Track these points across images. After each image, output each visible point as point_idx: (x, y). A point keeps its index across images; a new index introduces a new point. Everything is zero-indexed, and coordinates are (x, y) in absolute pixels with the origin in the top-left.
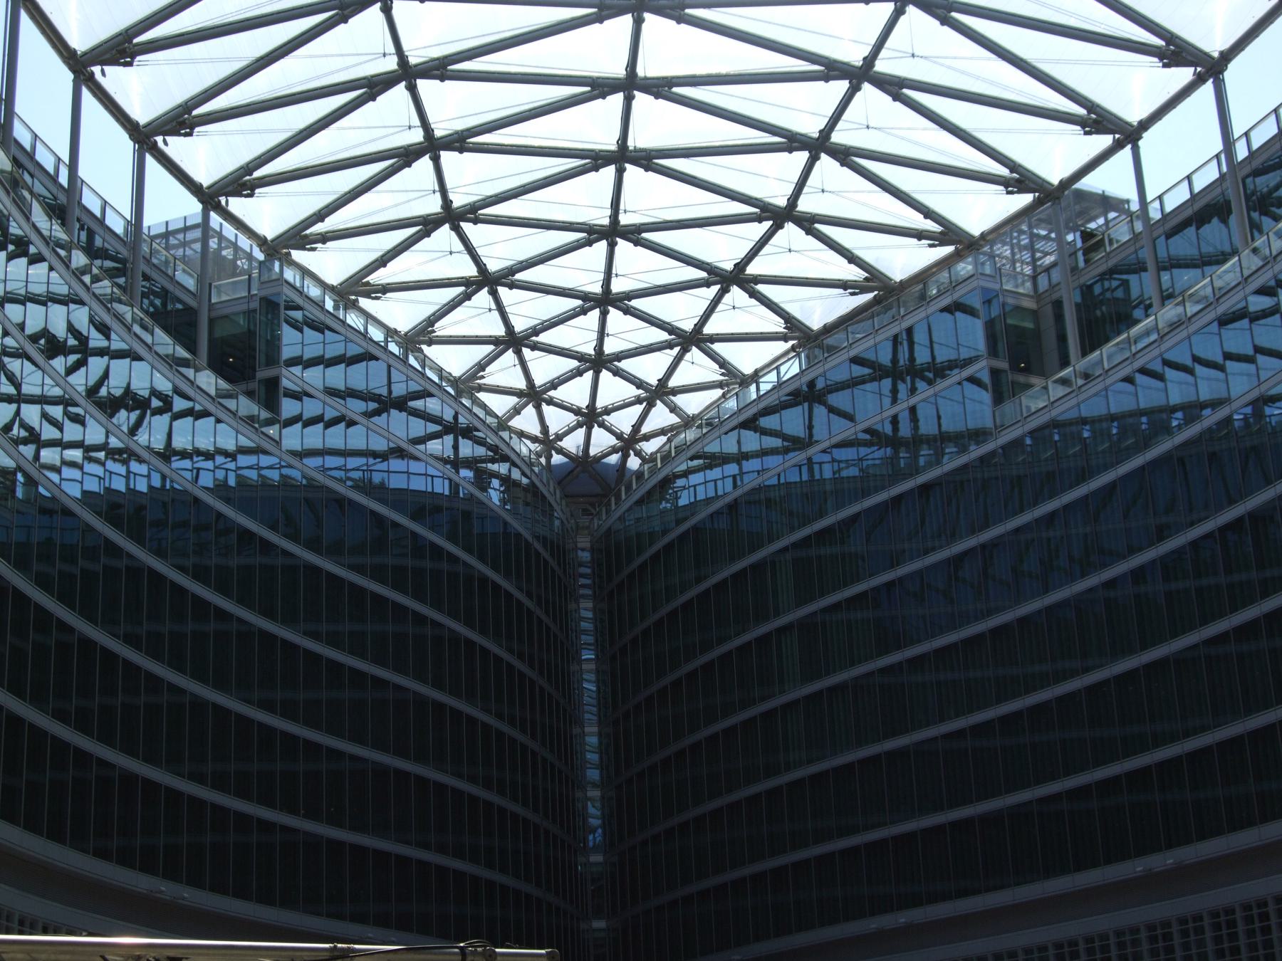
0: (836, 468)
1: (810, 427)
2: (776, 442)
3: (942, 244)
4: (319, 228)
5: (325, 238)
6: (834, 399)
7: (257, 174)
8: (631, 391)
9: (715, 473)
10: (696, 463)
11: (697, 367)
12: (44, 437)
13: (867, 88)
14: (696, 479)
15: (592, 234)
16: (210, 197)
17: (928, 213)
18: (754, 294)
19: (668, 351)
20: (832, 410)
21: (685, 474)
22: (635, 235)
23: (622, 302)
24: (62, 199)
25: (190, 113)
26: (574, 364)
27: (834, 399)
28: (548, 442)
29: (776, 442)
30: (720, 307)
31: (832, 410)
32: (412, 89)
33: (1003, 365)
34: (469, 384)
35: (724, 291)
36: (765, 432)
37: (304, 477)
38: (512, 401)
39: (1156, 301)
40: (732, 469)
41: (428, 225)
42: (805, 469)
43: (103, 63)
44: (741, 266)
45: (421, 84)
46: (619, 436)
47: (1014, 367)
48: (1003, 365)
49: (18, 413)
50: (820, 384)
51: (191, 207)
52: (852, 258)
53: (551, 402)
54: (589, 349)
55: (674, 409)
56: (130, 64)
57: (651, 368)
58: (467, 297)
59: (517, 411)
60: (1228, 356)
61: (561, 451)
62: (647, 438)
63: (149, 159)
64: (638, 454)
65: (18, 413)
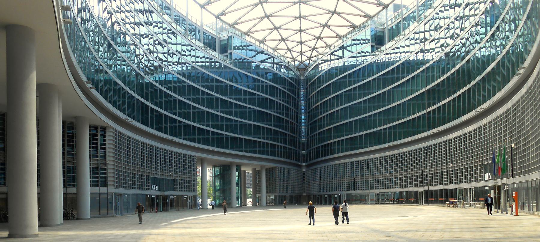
0: (348, 63)
1: (343, 54)
2: (337, 57)
6: (348, 48)
8: (309, 49)
9: (326, 64)
10: (322, 62)
11: (320, 43)
13: (335, 14)
14: (322, 65)
15: (296, 18)
20: (348, 50)
21: (320, 64)
22: (305, 17)
27: (348, 48)
28: (294, 59)
29: (337, 57)
31: (348, 50)
32: (262, 5)
33: (374, 44)
36: (335, 55)
38: (285, 51)
39: (75, 219)
40: (329, 63)
41: (262, 18)
42: (342, 63)
44: (326, 23)
47: (377, 44)
48: (374, 44)
49: (158, 55)
53: (292, 51)
57: (312, 44)
62: (313, 57)
64: (312, 60)
65: (158, 55)
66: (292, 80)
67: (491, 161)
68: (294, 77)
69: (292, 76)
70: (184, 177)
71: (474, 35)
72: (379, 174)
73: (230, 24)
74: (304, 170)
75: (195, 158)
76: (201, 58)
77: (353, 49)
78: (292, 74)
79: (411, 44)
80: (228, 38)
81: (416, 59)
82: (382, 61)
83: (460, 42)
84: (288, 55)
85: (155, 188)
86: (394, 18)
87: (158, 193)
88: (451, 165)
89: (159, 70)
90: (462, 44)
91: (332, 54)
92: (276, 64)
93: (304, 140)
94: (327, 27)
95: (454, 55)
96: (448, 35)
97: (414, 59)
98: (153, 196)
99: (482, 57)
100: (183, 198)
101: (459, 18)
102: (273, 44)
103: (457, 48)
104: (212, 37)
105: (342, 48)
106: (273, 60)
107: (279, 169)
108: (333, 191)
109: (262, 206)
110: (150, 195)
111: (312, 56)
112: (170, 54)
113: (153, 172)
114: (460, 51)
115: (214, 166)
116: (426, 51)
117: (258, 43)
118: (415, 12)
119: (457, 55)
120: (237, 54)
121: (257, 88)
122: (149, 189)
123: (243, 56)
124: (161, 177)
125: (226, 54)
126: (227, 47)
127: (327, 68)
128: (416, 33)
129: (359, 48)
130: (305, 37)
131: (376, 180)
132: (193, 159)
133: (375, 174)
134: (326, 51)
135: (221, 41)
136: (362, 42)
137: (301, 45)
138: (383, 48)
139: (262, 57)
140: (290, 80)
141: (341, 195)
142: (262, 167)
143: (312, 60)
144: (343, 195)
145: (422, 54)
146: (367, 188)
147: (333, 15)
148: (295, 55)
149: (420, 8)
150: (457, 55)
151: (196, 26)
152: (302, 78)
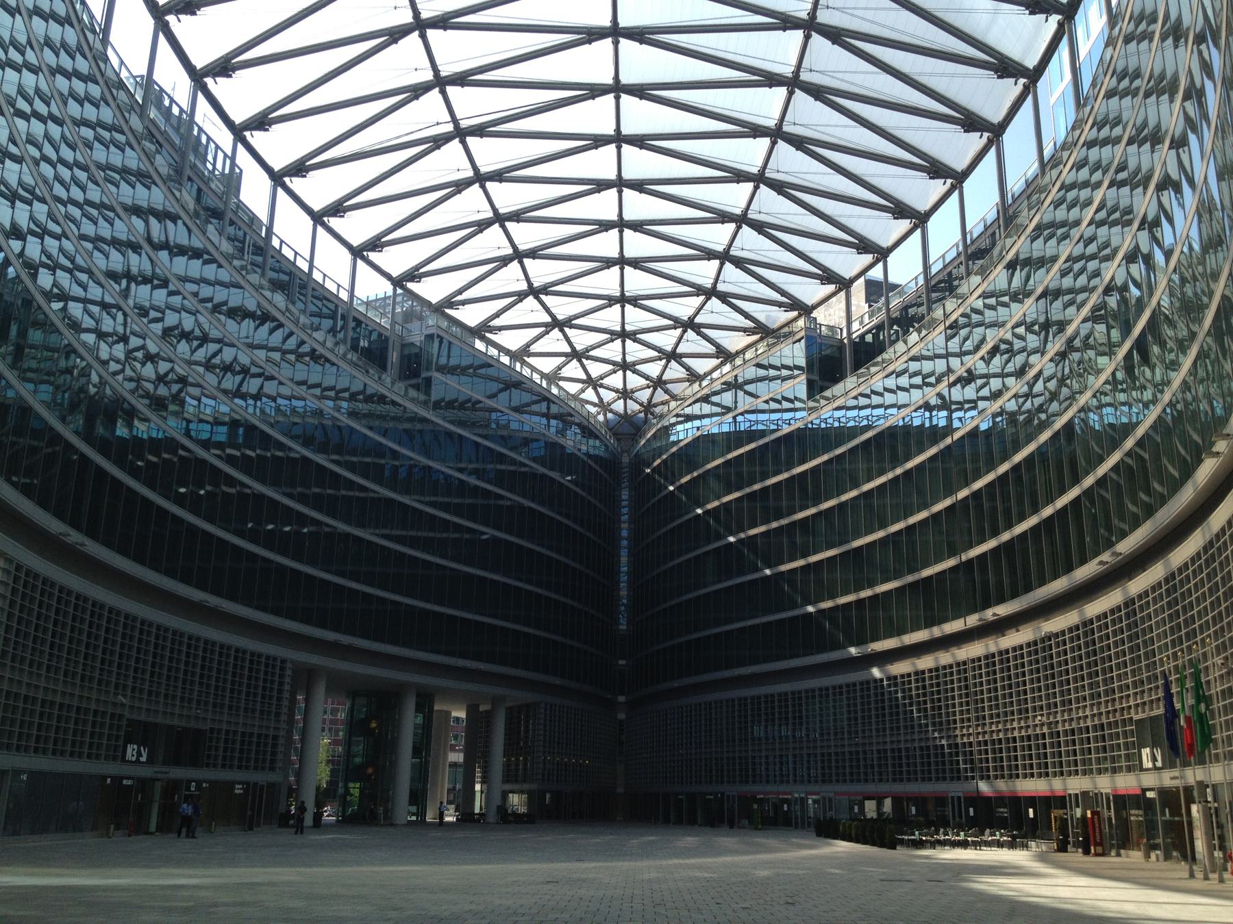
1: (736, 402)
3: (792, 310)
4: (459, 298)
5: (464, 303)
7: (422, 271)
8: (643, 382)
9: (688, 425)
10: (680, 419)
12: (84, 326)
14: (680, 427)
15: (611, 301)
16: (398, 282)
17: (783, 293)
18: (699, 333)
19: (658, 362)
20: (747, 393)
23: (633, 336)
24: (262, 244)
25: (380, 240)
26: (611, 367)
27: (747, 388)
28: (603, 406)
30: (702, 312)
31: (747, 393)
33: (816, 377)
34: (553, 377)
35: (684, 332)
37: (259, 305)
38: (580, 386)
40: (697, 423)
43: (291, 176)
44: (692, 319)
45: (469, 140)
46: (641, 404)
50: (740, 380)
51: (386, 288)
52: (747, 316)
54: (619, 359)
55: (667, 391)
56: (305, 176)
58: (547, 333)
59: (583, 391)
60: (886, 389)
61: (611, 411)
63: (279, 189)
66: (596, 463)
67: (354, 739)
68: (601, 454)
69: (597, 452)
70: (229, 723)
71: (1082, 371)
72: (874, 733)
73: (434, 302)
74: (622, 716)
75: (289, 665)
76: (311, 387)
77: (761, 388)
78: (587, 446)
79: (912, 386)
80: (423, 338)
81: (927, 425)
82: (823, 425)
83: (1045, 388)
84: (590, 395)
85: (139, 754)
86: (867, 315)
87: (146, 772)
88: (1039, 718)
89: (172, 408)
90: (1051, 393)
91: (705, 399)
92: (555, 417)
93: (625, 627)
94: (693, 329)
95: (1029, 421)
96: (1010, 368)
97: (923, 425)
98: (125, 782)
99: (1107, 428)
100: (234, 788)
101: (1036, 328)
102: (547, 365)
103: (1038, 401)
104: (380, 335)
105: (733, 385)
106: (548, 408)
107: (546, 709)
108: (701, 783)
109: (392, 825)
110: (117, 779)
111: (654, 401)
112: (215, 367)
113: (137, 704)
114: (1045, 411)
115: (353, 694)
116: (953, 407)
117: (505, 360)
118: (922, 304)
119: (1036, 422)
120: (446, 386)
121: (500, 479)
122: (114, 758)
123: (474, 395)
124: (168, 722)
125: (414, 381)
126: (419, 364)
127: (691, 435)
128: (913, 359)
129: (777, 388)
130: (635, 351)
131: (823, 754)
132: (282, 669)
133: (864, 731)
134: (689, 392)
135: (403, 346)
136: (785, 372)
137: (624, 372)
138: (838, 389)
139: (518, 397)
140: (589, 462)
141: (723, 794)
142: (496, 701)
143: (652, 414)
144: (728, 796)
145: (944, 413)
146: (827, 778)
147: (708, 299)
148: (608, 396)
149: (934, 295)
150: (1036, 422)
151: (336, 301)
152: (626, 459)
